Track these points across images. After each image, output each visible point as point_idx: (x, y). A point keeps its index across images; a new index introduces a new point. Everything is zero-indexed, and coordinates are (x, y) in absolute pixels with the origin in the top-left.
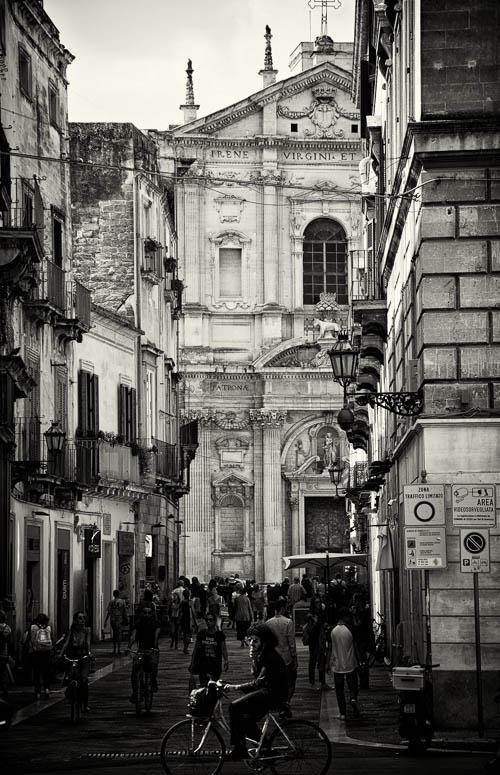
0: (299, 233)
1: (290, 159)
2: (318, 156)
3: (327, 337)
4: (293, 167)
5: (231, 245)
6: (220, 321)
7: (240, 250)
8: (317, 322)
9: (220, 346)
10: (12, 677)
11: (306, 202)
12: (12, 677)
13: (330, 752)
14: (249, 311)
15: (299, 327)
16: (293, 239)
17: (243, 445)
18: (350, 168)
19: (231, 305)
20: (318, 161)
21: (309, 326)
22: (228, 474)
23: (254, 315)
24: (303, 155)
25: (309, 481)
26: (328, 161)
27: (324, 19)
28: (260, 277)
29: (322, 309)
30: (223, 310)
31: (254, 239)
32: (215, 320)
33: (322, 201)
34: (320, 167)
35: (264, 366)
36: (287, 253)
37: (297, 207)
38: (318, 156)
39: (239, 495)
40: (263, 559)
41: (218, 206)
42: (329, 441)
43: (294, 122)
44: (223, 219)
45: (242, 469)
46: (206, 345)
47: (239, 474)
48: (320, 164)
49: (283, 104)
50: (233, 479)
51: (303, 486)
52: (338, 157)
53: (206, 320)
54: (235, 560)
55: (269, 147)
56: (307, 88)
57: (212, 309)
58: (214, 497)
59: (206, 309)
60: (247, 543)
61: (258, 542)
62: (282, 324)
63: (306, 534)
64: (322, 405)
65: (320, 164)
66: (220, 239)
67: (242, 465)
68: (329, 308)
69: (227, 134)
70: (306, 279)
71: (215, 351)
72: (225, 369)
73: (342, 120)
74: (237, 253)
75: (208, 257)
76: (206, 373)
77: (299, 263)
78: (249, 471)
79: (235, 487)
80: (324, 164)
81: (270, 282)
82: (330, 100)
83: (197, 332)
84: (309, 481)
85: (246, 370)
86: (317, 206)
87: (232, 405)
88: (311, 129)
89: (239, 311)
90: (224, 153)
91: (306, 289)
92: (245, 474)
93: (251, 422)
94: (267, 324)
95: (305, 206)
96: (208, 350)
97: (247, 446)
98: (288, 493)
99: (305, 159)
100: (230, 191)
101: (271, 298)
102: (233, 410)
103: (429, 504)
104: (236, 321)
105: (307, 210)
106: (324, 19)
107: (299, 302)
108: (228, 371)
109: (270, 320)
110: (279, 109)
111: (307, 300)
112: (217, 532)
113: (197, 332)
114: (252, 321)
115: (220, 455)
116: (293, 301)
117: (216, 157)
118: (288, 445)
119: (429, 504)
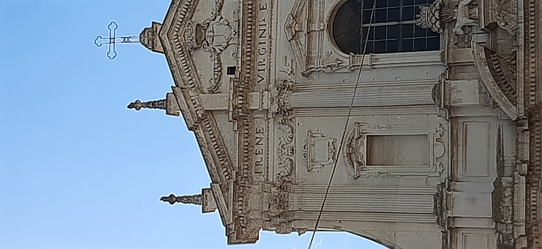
0: (346, 59)
2: (262, 40)
4: (273, 71)
5: (363, 150)
6: (460, 164)
7: (370, 138)
9: (494, 165)
11: (309, 52)
13: (513, 236)
14: (447, 126)
16: (353, 69)
19: (439, 150)
20: (266, 40)
23: (451, 118)
24: (260, 59)
27: (126, 40)
28: (402, 110)
30: (446, 161)
32: (459, 174)
37: (316, 65)
38: (262, 40)
43: (225, 70)
49: (206, 87)
55: (246, 101)
57: (445, 175)
59: (443, 185)
68: (437, 14)
69: (234, 153)
72: (524, 162)
74: (376, 142)
77: (384, 58)
81: (406, 97)
83: (473, 200)
86: (315, 36)
88: (231, 49)
89: (446, 138)
90: (258, 158)
91: (420, 48)
94: (460, 100)
95: (314, 54)
96: (498, 184)
99: (265, 56)
103: (117, 25)
104: (460, 142)
106: (126, 40)
107: (434, 56)
108: (527, 157)
109: (454, 96)
111: (434, 45)
113: (473, 200)
116: (433, 64)
117: (262, 169)
119: (95, 41)
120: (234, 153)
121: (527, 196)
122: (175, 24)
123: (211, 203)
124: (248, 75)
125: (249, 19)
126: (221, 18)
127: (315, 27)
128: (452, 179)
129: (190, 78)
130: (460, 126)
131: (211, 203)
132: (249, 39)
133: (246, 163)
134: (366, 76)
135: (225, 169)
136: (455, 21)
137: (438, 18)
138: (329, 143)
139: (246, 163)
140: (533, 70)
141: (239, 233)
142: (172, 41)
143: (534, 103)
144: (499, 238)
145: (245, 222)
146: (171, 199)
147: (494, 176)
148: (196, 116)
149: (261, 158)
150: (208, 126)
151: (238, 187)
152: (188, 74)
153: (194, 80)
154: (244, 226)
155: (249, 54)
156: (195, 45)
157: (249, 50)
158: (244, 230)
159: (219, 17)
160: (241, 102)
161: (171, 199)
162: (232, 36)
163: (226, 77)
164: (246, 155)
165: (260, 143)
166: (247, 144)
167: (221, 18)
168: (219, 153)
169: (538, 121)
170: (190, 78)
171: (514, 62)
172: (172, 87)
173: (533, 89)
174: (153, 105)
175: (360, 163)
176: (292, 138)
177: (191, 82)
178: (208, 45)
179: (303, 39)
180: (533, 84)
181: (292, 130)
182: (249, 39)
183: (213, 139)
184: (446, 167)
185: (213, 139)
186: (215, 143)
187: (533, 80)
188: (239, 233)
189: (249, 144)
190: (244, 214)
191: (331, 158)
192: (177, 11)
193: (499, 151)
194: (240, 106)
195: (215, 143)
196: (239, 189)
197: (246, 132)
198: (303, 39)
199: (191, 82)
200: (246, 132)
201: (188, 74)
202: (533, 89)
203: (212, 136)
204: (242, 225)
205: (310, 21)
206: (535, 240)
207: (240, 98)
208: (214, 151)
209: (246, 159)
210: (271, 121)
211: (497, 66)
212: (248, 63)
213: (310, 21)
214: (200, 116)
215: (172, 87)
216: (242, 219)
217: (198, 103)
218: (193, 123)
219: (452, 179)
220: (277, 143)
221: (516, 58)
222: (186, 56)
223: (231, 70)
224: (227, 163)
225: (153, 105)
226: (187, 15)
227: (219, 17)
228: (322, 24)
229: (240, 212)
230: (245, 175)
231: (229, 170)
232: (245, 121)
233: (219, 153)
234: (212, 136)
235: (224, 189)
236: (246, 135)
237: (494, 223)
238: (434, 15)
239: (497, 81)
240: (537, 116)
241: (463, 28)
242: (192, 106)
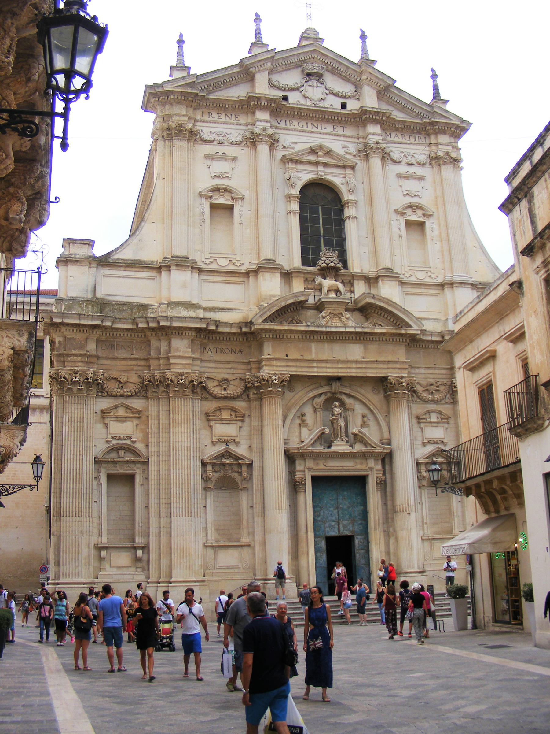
0: (296, 191)
1: (282, 125)
3: (331, 296)
5: (222, 201)
8: (319, 280)
10: (5, 665)
12: (5, 665)
14: (243, 269)
15: (298, 286)
16: (289, 197)
17: (240, 417)
18: (342, 138)
19: (223, 262)
21: (308, 280)
22: (221, 448)
25: (317, 456)
26: (319, 130)
29: (324, 265)
30: (214, 267)
31: (247, 197)
32: (205, 277)
33: (316, 164)
34: (312, 135)
35: (265, 321)
36: (283, 212)
39: (235, 475)
40: (264, 550)
41: (209, 162)
42: (337, 411)
44: (213, 175)
45: (237, 444)
46: (195, 301)
47: (232, 447)
48: (312, 132)
49: (276, 78)
50: (227, 454)
51: (310, 463)
52: (329, 128)
53: (196, 275)
54: (231, 551)
56: (297, 66)
57: (203, 266)
58: (205, 479)
60: (245, 531)
61: (258, 530)
62: (281, 283)
63: (315, 521)
64: (329, 370)
65: (312, 132)
66: (211, 194)
67: (237, 440)
68: (332, 265)
69: (221, 95)
70: (304, 241)
71: (205, 309)
73: (331, 97)
75: (198, 211)
76: (196, 329)
78: (246, 447)
79: (230, 464)
80: (317, 133)
81: (255, 318)
82: (319, 76)
84: (317, 456)
85: (241, 328)
86: (313, 168)
87: (225, 371)
89: (232, 268)
91: (304, 251)
92: (241, 450)
93: (247, 389)
95: (300, 167)
96: (197, 306)
97: (243, 416)
98: (292, 473)
100: (221, 149)
101: (267, 254)
102: (226, 376)
105: (303, 171)
106: (310, 17)
107: (297, 262)
110: (270, 81)
111: (305, 262)
112: (209, 520)
114: (245, 280)
115: (211, 427)
118: (291, 416)
120: (221, 95)
121: (190, 329)
122: (323, 57)
123: (178, 74)
124: (282, 112)
125: (327, 117)
126: (327, 94)
127: (321, 168)
128: (200, 271)
129: (281, 64)
130: (241, 279)
131: (178, 74)
132: (311, 115)
133: (211, 105)
134: (282, 207)
135: (206, 87)
136: (325, 279)
137: (329, 265)
138: (228, 173)
139: (211, 105)
140: (289, 337)
141: (154, 95)
142: (310, 53)
143: (264, 336)
144: (154, 305)
145: (163, 101)
146: (181, 42)
147: (204, 304)
148: (251, 66)
149: (214, 118)
150: (242, 76)
151: (193, 96)
152: (284, 63)
153: (279, 68)
154: (160, 99)
155: (299, 114)
156: (307, 71)
157: (303, 114)
158: (157, 99)
159: (327, 92)
160: (263, 104)
161: (181, 42)
162: (313, 102)
163: (280, 94)
164: (218, 105)
165: (227, 117)
166: (227, 106)
167: (327, 94)
168: (220, 83)
169: (247, 339)
170: (281, 64)
171: (294, 322)
172: (275, 49)
173: (275, 336)
174: (258, 33)
175: (211, 197)
176: (231, 143)
177: (278, 65)
178: (306, 82)
179: (312, 158)
180: (278, 337)
181: (238, 144)
182: (311, 115)
183: (231, 79)
184: (210, 266)
185: (231, 79)
186: (228, 80)
187: (281, 337)
188: (154, 95)
189: (227, 108)
190: (170, 101)
191: (215, 174)
192: (334, 59)
193: (223, 309)
194: (259, 103)
195: (228, 80)
196: (191, 97)
197: (237, 106)
198: (312, 158)
199: (278, 65)
200: (237, 106)
201: (284, 63)
202: (275, 336)
203: (234, 79)
204: (161, 98)
205: (325, 165)
206: (154, 334)
207: (266, 104)
208: (221, 80)
209: (215, 105)
210: (245, 128)
211: (292, 309)
212: (292, 113)
213: (325, 165)
214: (251, 69)
215: (275, 49)
216: (166, 98)
217: (261, 69)
218: (246, 63)
219: (200, 271)
220: (228, 131)
221: (297, 323)
222: (298, 63)
223: (285, 98)
224: (211, 89)
225: (258, 33)
226: (330, 67)
227: (327, 92)
228: (323, 174)
229: (172, 97)
230: (201, 103)
231: (205, 91)
232: (246, 106)
233: (220, 83)
234: (234, 79)
235: (191, 85)
236: (234, 106)
237: (167, 302)
238: (331, 262)
239: (281, 309)
240: (252, 339)
241: (320, 284)
242: (259, 64)
